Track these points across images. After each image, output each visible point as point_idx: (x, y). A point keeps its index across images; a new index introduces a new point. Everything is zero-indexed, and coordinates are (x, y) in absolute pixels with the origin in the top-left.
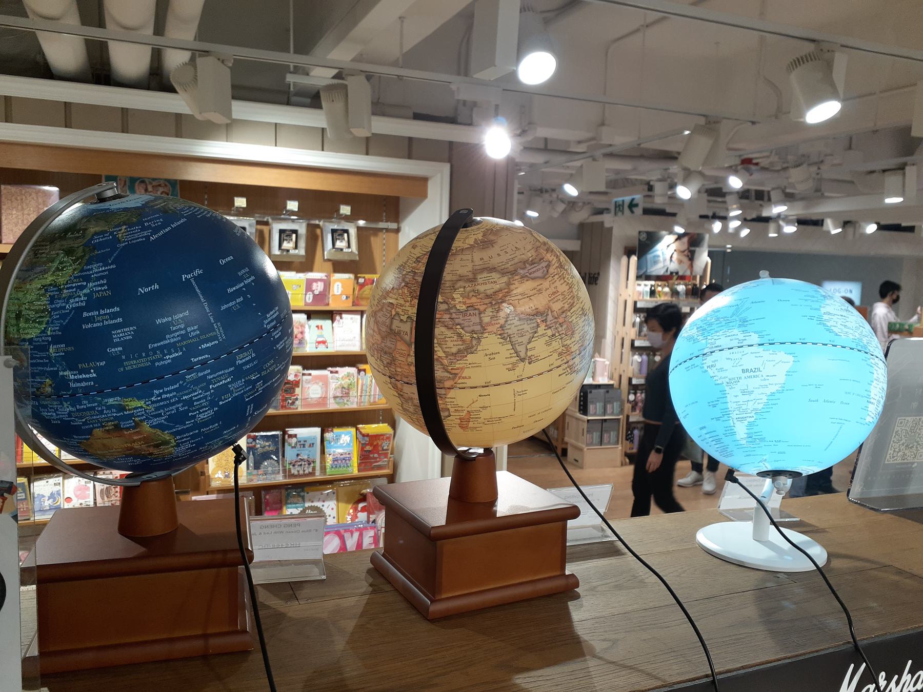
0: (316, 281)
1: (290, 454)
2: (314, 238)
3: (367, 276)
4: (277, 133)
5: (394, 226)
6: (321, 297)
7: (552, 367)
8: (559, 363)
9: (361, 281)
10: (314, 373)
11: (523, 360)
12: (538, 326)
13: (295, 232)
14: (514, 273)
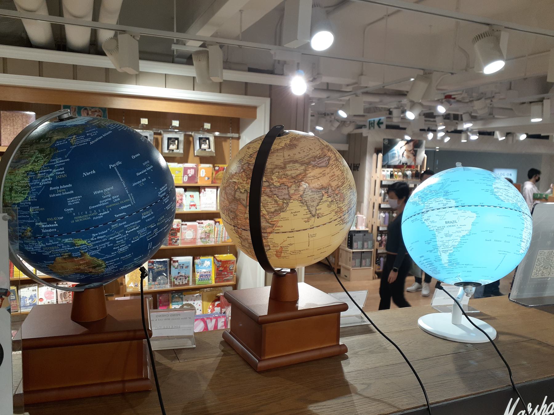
0: (190, 168)
1: (174, 273)
2: (188, 143)
3: (221, 166)
4: (166, 79)
5: (236, 135)
6: (193, 178)
7: (331, 220)
8: (335, 217)
9: (217, 168)
10: (189, 223)
11: (314, 216)
12: (323, 195)
13: (177, 139)
14: (308, 164)
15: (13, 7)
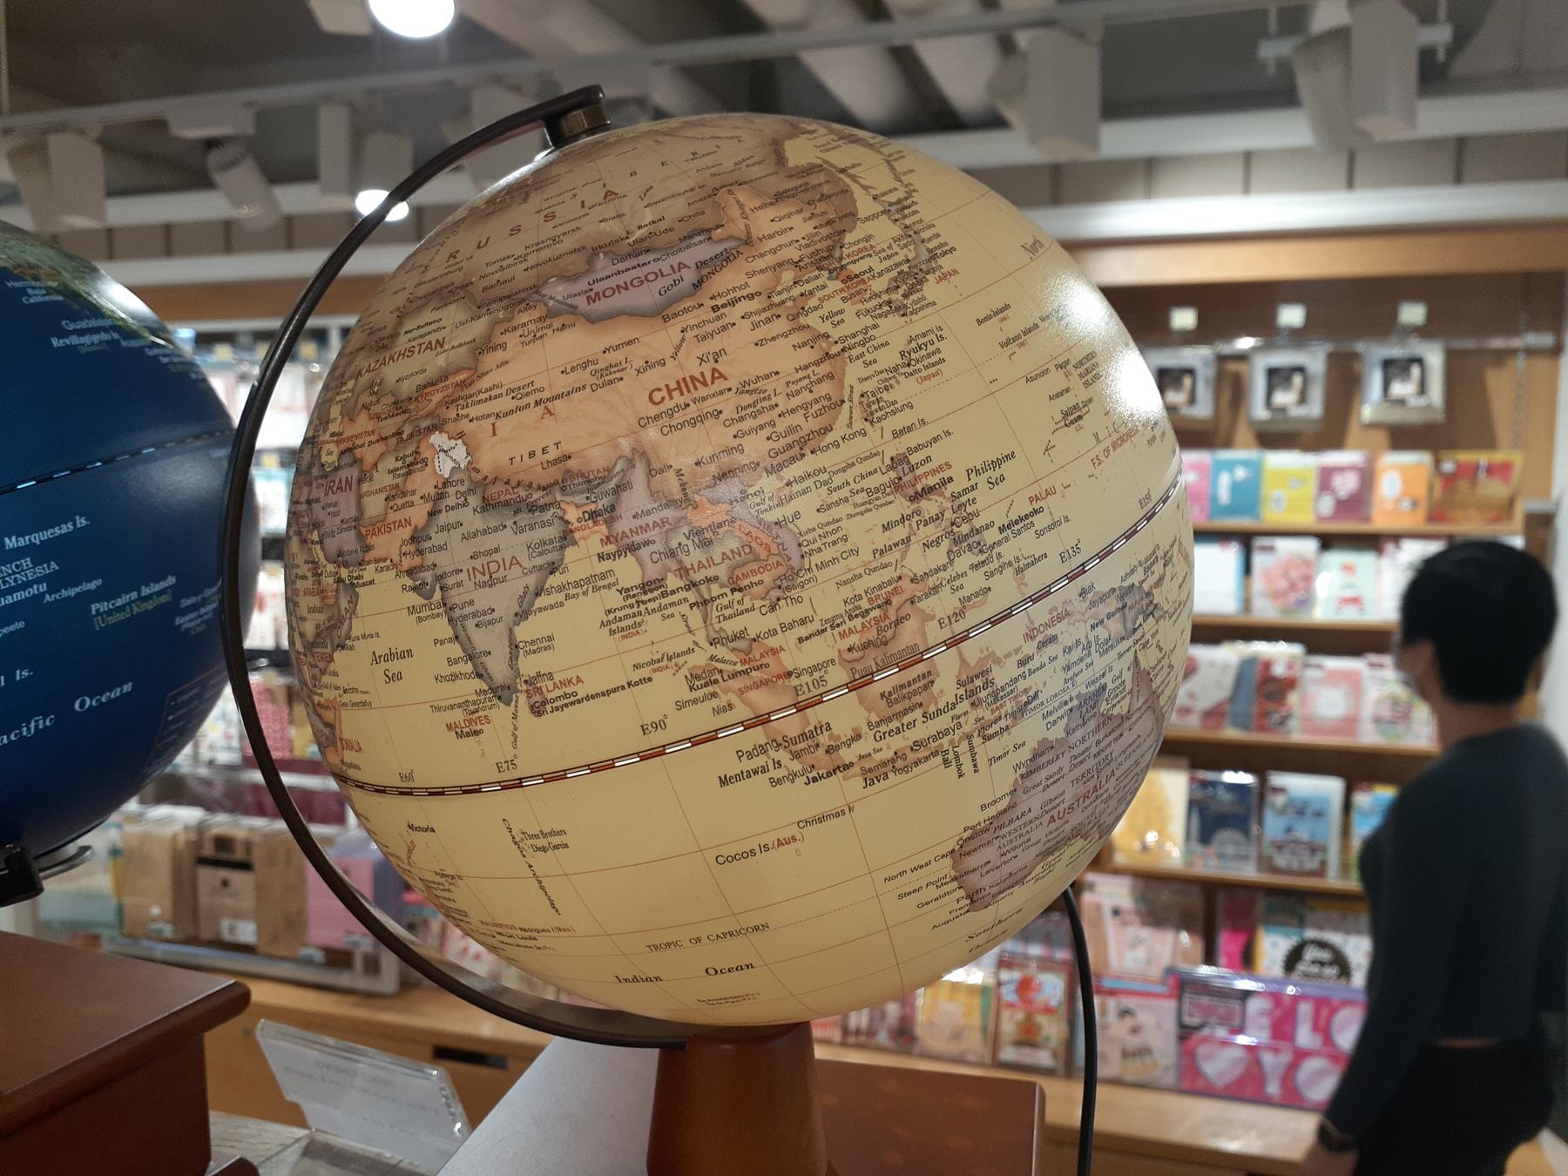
0: (1341, 469)
1: (1273, 826)
2: (1344, 384)
3: (1466, 457)
4: (1248, 170)
5: (1547, 340)
6: (1356, 504)
7: (657, 739)
8: (701, 718)
9: (1448, 467)
10: (1333, 663)
11: (502, 693)
12: (567, 538)
13: (1300, 369)
14: (517, 300)
15: (753, 24)
